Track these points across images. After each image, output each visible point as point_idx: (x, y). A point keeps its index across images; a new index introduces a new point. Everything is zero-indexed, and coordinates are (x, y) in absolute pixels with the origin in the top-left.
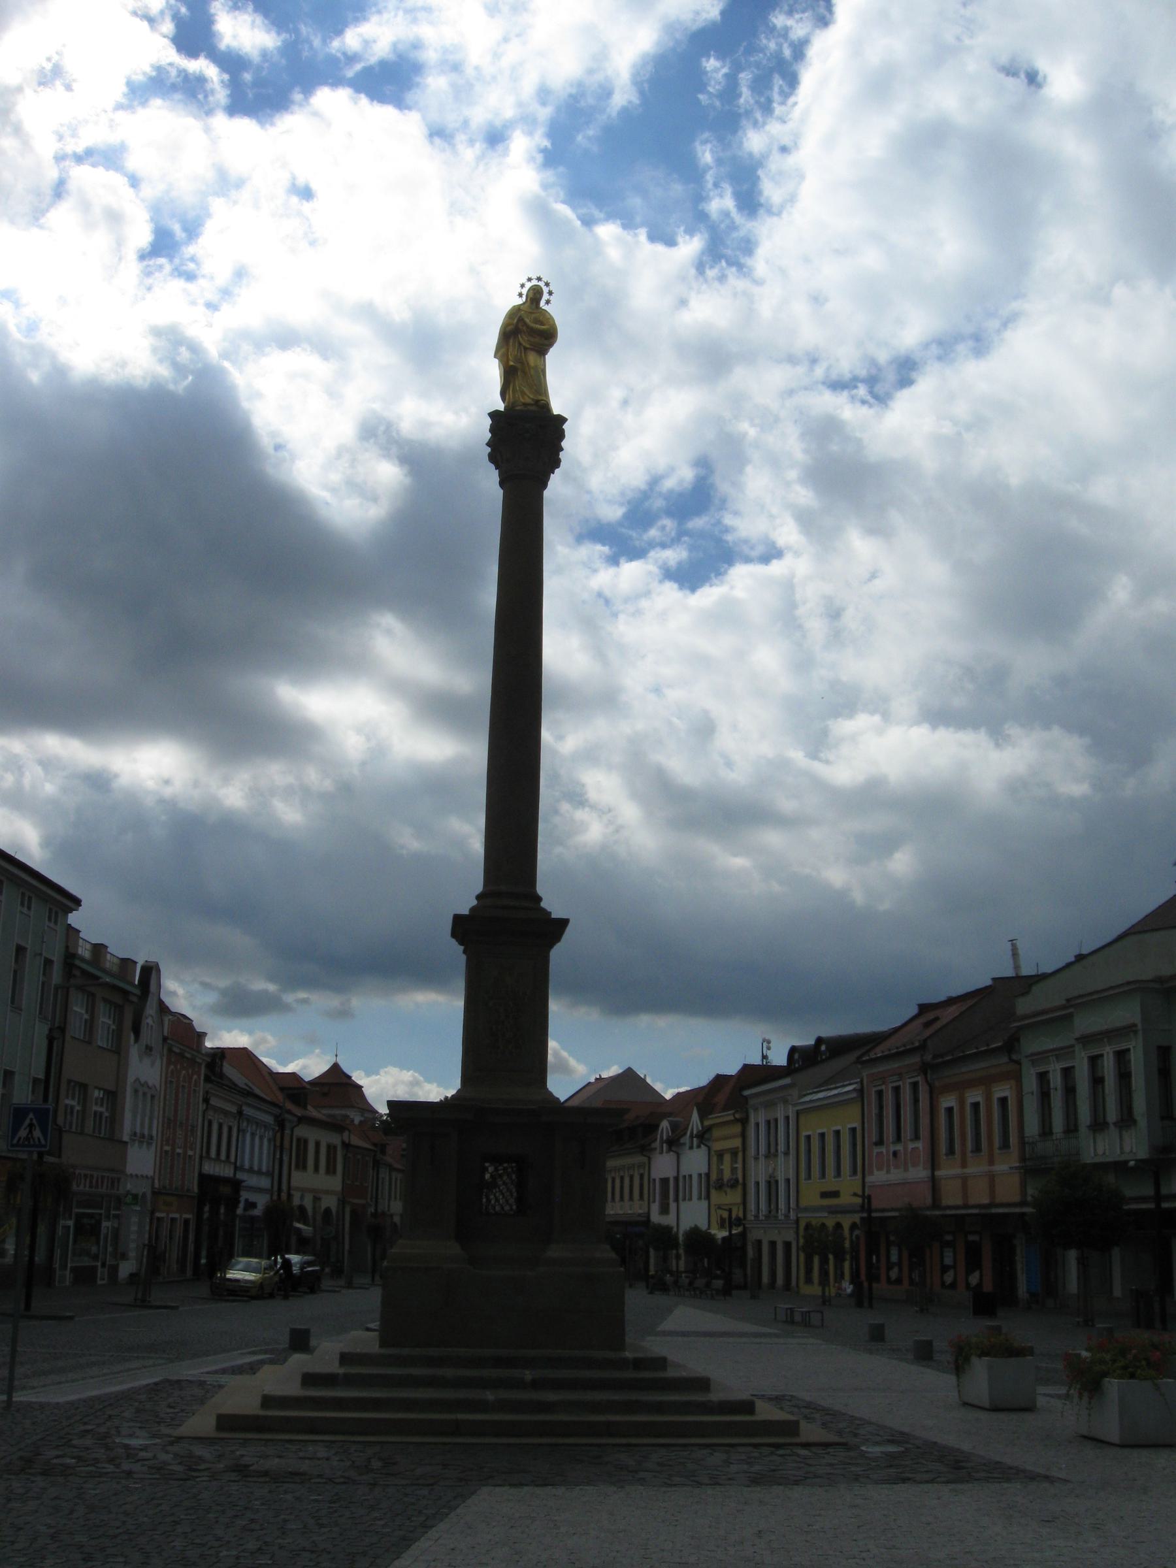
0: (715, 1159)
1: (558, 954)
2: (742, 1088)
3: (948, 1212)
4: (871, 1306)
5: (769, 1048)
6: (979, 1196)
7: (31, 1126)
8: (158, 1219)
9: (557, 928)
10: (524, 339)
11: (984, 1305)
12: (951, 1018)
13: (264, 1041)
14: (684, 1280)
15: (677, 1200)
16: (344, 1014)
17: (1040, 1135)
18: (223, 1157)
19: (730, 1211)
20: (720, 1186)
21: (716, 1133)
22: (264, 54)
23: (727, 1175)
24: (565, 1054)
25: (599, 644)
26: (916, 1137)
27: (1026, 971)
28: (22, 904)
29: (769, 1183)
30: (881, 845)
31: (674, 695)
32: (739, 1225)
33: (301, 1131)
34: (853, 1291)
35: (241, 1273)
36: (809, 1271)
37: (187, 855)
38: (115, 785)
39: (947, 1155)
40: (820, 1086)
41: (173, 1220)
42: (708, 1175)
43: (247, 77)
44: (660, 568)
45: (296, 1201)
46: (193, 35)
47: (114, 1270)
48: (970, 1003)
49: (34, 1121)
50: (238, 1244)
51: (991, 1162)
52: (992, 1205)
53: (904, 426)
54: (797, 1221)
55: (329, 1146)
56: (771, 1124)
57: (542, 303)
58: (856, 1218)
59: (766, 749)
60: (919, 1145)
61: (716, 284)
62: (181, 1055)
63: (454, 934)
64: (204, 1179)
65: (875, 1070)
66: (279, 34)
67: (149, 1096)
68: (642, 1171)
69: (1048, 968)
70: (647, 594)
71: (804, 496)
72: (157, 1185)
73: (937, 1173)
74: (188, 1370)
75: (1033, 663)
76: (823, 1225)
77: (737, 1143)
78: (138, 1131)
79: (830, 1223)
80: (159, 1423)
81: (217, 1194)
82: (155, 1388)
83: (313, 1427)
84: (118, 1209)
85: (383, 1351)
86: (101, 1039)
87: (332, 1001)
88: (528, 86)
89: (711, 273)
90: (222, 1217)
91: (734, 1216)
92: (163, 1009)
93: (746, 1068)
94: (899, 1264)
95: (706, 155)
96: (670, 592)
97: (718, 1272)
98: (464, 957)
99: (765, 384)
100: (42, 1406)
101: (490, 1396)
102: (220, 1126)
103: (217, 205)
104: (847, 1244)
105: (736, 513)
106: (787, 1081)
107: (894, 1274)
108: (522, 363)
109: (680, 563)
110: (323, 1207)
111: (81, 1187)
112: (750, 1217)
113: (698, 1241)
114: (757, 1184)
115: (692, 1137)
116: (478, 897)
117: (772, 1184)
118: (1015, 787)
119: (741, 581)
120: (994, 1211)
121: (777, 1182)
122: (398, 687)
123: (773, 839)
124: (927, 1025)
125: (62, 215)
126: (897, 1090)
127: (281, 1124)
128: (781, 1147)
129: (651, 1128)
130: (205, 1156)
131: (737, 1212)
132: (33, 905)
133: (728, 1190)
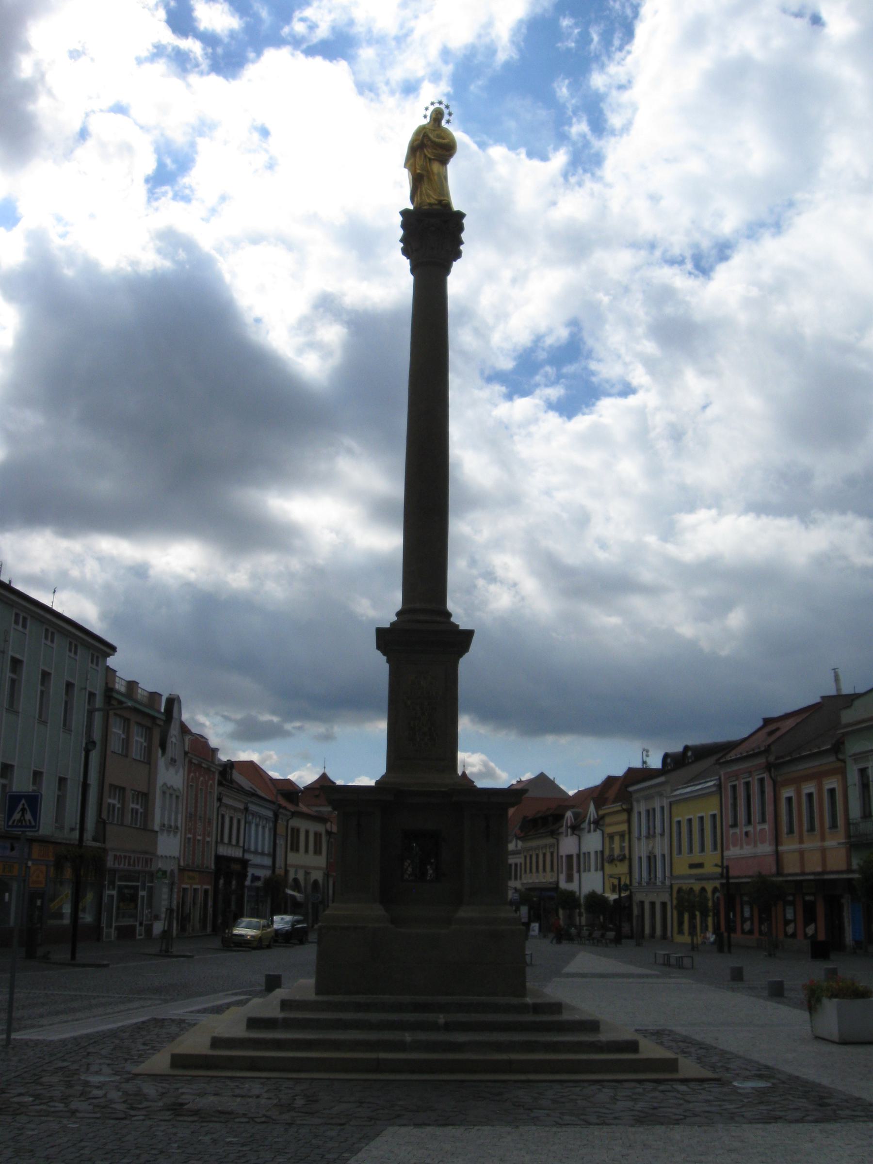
0: (607, 840)
1: (465, 664)
2: (627, 786)
3: (790, 878)
4: (730, 951)
5: (647, 756)
6: (814, 865)
7: (23, 810)
8: (184, 889)
9: (462, 640)
10: (428, 152)
11: (820, 951)
12: (787, 729)
13: (270, 757)
14: (585, 932)
15: (579, 871)
16: (328, 737)
17: (862, 818)
18: (234, 842)
19: (619, 879)
20: (612, 860)
21: (608, 820)
22: (232, 34)
23: (617, 852)
24: (492, 764)
25: (504, 459)
26: (763, 820)
27: (847, 690)
28: (70, 650)
29: (649, 858)
30: (719, 606)
31: (561, 496)
32: (626, 890)
33: (295, 823)
34: (715, 940)
35: (245, 929)
36: (681, 923)
37: (205, 623)
38: (151, 572)
39: (787, 834)
40: (686, 783)
41: (195, 890)
42: (602, 852)
43: (220, 51)
44: (545, 402)
45: (291, 876)
46: (181, 20)
47: (149, 929)
48: (798, 719)
49: (26, 806)
50: (246, 908)
51: (823, 839)
52: (824, 872)
53: (725, 290)
54: (671, 887)
55: (316, 834)
56: (650, 813)
57: (443, 123)
58: (717, 883)
59: (629, 536)
60: (766, 827)
61: (577, 188)
62: (199, 766)
63: (379, 647)
64: (219, 859)
65: (729, 770)
66: (241, 18)
67: (174, 797)
68: (552, 850)
69: (861, 690)
70: (536, 421)
71: (650, 347)
72: (182, 864)
73: (780, 848)
74: (177, 1010)
75: (829, 467)
76: (691, 889)
77: (624, 827)
78: (166, 823)
79: (697, 888)
80: (126, 1060)
81: (229, 870)
82: (139, 1028)
83: (253, 1065)
84: (152, 882)
85: (320, 998)
86: (136, 752)
87: (320, 728)
88: (433, 52)
89: (573, 180)
90: (233, 887)
91: (622, 883)
92: (184, 729)
93: (631, 771)
94: (751, 919)
95: (563, 90)
96: (553, 419)
97: (611, 926)
98: (387, 665)
99: (618, 262)
100: (37, 1043)
101: (408, 1037)
102: (231, 819)
103: (202, 144)
104: (710, 904)
105: (599, 360)
106: (662, 779)
107: (747, 926)
108: (427, 171)
109: (559, 399)
110: (312, 880)
111: (122, 866)
112: (635, 884)
113: (595, 902)
114: (640, 858)
115: (590, 823)
116: (398, 614)
117: (651, 858)
118: (821, 561)
119: (608, 411)
120: (826, 877)
121: (655, 856)
122: (355, 495)
123: (638, 603)
124: (771, 733)
125: (86, 152)
126: (747, 784)
127: (276, 816)
128: (658, 830)
129: (558, 817)
130: (220, 841)
131: (625, 880)
132: (79, 652)
133: (618, 864)
